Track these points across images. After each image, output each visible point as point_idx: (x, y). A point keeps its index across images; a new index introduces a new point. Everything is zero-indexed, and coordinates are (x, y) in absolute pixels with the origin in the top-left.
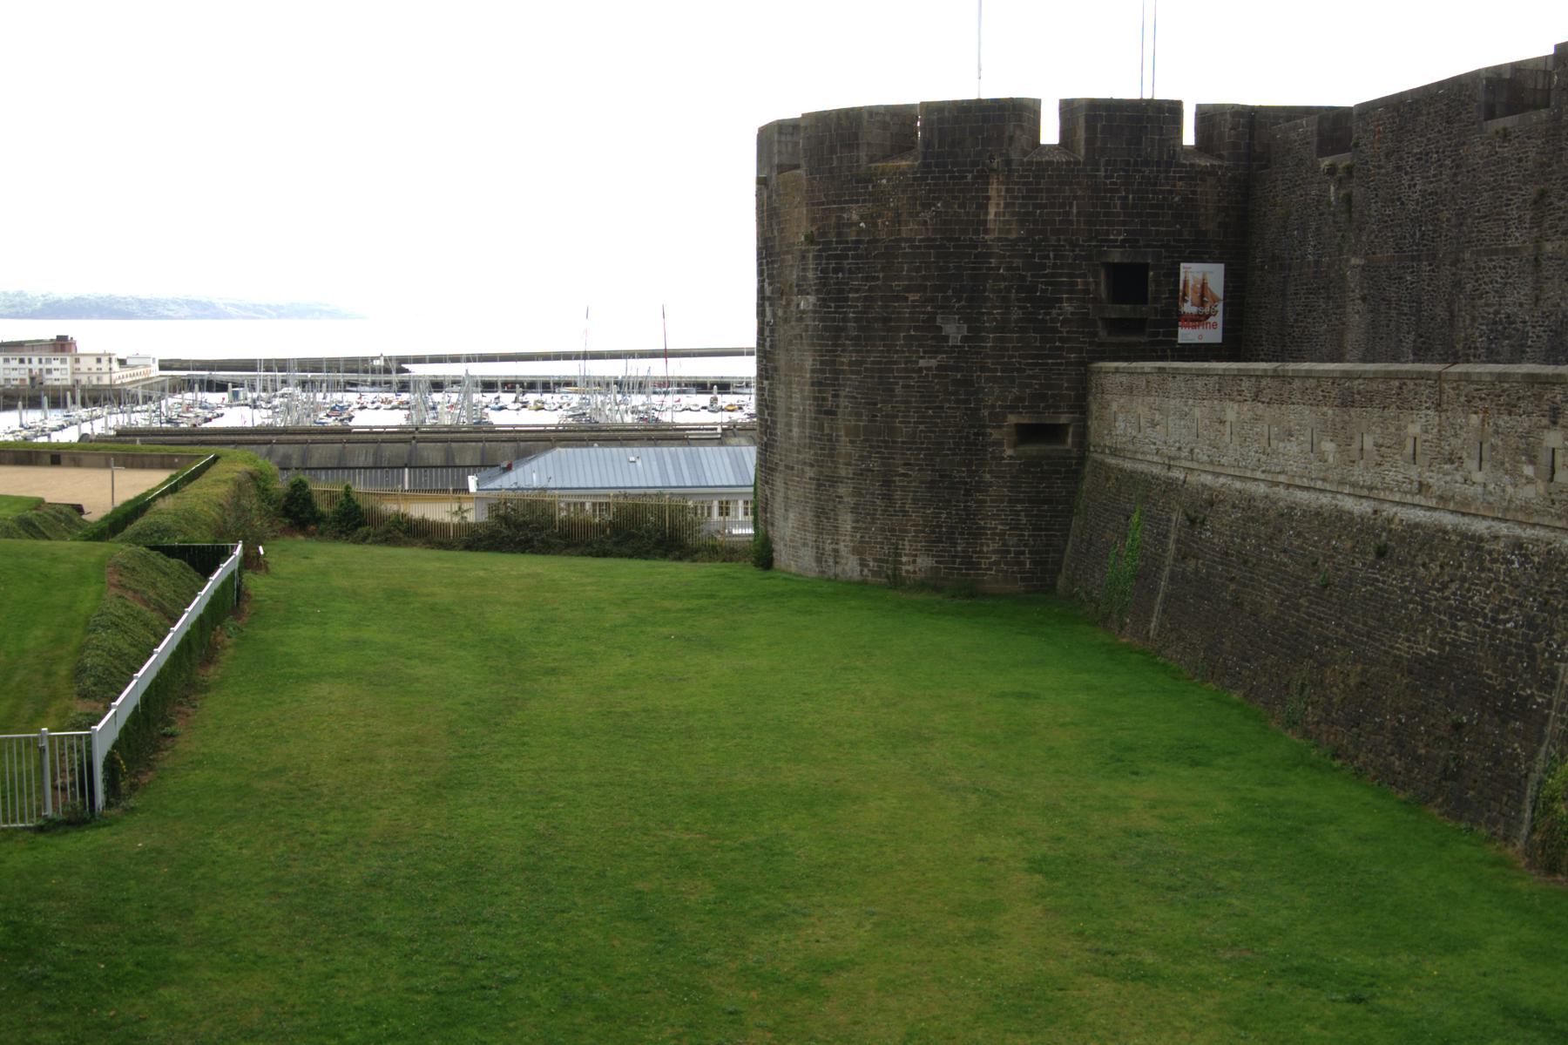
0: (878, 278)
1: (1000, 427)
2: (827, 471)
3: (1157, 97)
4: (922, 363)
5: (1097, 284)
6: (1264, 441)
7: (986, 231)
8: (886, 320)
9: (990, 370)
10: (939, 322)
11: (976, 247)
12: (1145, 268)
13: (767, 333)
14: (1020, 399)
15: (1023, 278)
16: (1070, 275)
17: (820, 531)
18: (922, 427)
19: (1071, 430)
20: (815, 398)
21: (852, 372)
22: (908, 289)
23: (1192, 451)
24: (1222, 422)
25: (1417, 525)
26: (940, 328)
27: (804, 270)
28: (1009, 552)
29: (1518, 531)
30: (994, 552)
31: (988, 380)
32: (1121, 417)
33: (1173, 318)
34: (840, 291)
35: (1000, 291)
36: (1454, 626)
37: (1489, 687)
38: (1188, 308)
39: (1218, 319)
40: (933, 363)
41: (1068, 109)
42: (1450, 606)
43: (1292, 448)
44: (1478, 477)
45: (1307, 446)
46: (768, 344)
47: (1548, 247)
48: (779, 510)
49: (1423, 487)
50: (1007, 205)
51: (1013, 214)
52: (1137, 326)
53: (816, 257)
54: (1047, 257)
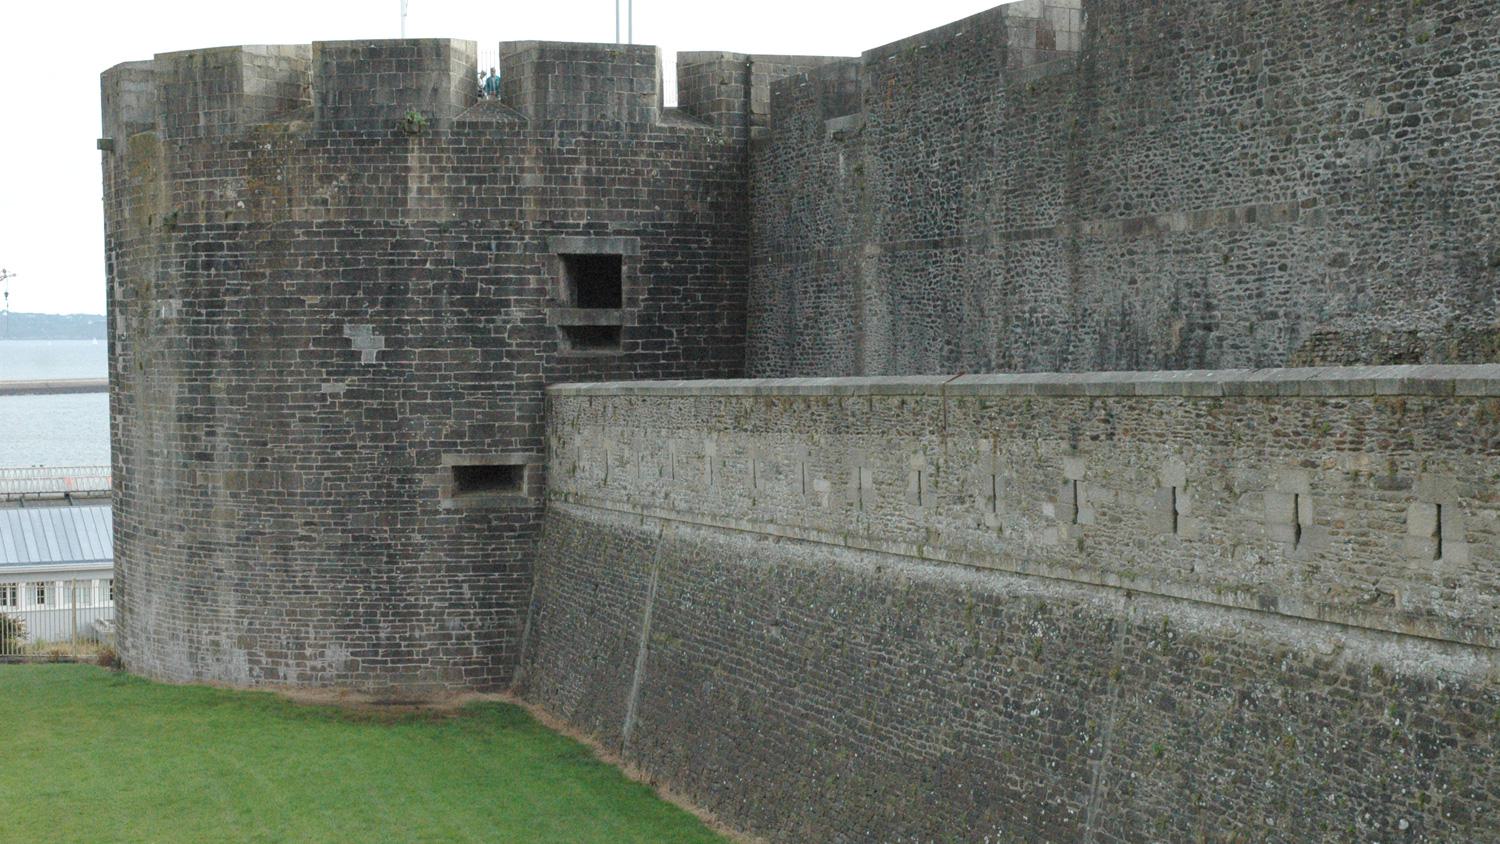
0: (263, 275)
1: (433, 471)
3: (635, 41)
4: (326, 388)
5: (555, 281)
6: (749, 482)
7: (406, 213)
9: (415, 395)
10: (347, 331)
11: (394, 234)
12: (615, 261)
13: (119, 350)
15: (456, 275)
16: (518, 271)
18: (327, 473)
19: (526, 473)
20: (184, 438)
21: (232, 402)
23: (667, 496)
24: (700, 457)
25: (925, 586)
26: (348, 342)
27: (165, 265)
28: (449, 637)
29: (1041, 590)
30: (430, 637)
32: (585, 454)
34: (214, 293)
35: (427, 292)
36: (971, 717)
37: (1016, 795)
40: (341, 388)
42: (966, 690)
44: (990, 520)
45: (798, 486)
46: (120, 366)
47: (1087, 228)
49: (930, 535)
51: (441, 191)
52: (608, 335)
53: (179, 248)
54: (489, 248)
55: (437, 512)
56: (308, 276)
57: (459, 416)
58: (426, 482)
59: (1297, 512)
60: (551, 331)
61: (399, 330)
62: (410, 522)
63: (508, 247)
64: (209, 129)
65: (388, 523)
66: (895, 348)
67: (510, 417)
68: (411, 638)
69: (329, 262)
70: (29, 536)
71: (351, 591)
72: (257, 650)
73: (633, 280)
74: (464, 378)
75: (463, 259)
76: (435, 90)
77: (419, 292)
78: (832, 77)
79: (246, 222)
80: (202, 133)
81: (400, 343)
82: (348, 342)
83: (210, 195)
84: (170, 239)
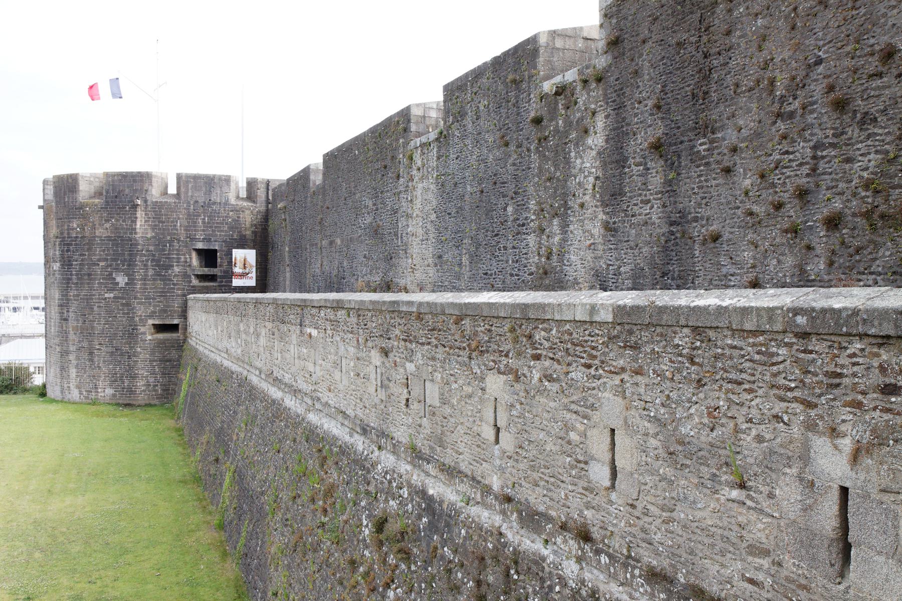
2: (65, 348)
4: (107, 295)
5: (191, 258)
8: (89, 275)
10: (114, 275)
12: (216, 251)
16: (177, 254)
17: (62, 378)
22: (99, 260)
26: (114, 279)
31: (138, 303)
33: (229, 275)
38: (237, 270)
39: (254, 275)
40: (112, 295)
50: (146, 221)
52: (212, 278)
53: (60, 244)
57: (155, 306)
59: (29, 337)
69: (108, 250)
72: (83, 390)
73: (222, 258)
74: (157, 292)
76: (146, 191)
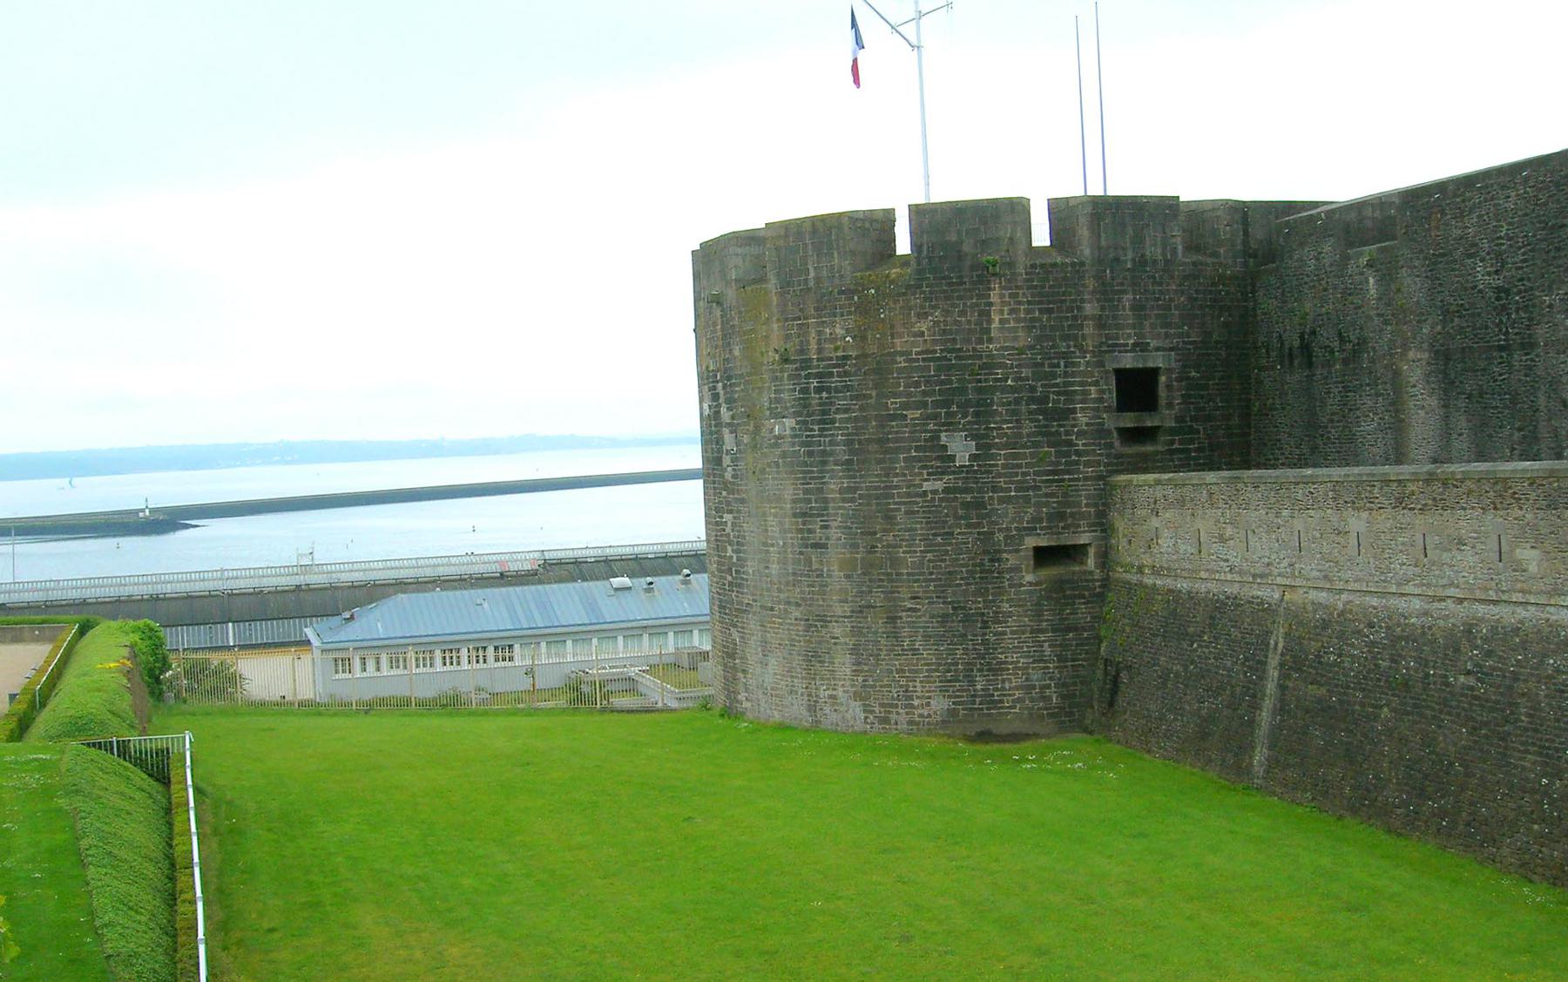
0: (870, 397)
1: (1017, 551)
3: (1115, 190)
4: (927, 486)
7: (990, 340)
9: (1002, 490)
12: (1155, 372)
14: (1035, 520)
15: (1032, 389)
16: (1082, 384)
17: (811, 677)
19: (1092, 551)
20: (800, 531)
21: (844, 500)
22: (905, 406)
26: (945, 447)
30: (1017, 688)
31: (1001, 501)
40: (939, 485)
41: (917, 212)
43: (1468, 558)
48: (753, 653)
51: (1017, 320)
55: (1022, 585)
56: (910, 395)
57: (1039, 505)
58: (1011, 560)
60: (1109, 432)
61: (986, 436)
62: (1000, 594)
63: (1074, 364)
64: (818, 279)
65: (982, 595)
66: (1446, 434)
67: (1079, 505)
68: (1003, 689)
70: (518, 608)
71: (952, 652)
75: (1037, 376)
77: (1003, 405)
78: (1353, 215)
79: (854, 354)
80: (811, 284)
81: (989, 446)
82: (945, 447)
83: (819, 333)
84: (782, 371)
